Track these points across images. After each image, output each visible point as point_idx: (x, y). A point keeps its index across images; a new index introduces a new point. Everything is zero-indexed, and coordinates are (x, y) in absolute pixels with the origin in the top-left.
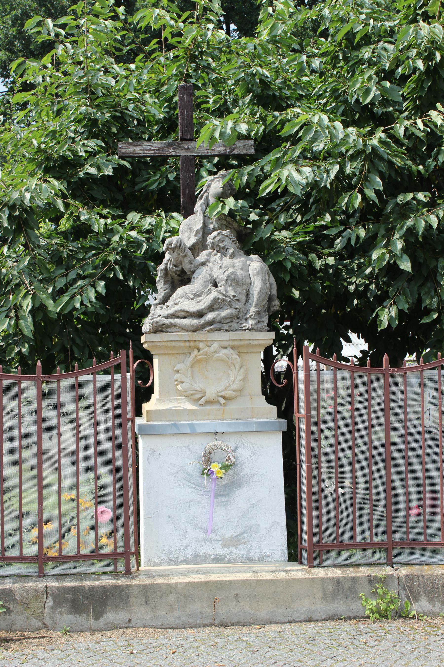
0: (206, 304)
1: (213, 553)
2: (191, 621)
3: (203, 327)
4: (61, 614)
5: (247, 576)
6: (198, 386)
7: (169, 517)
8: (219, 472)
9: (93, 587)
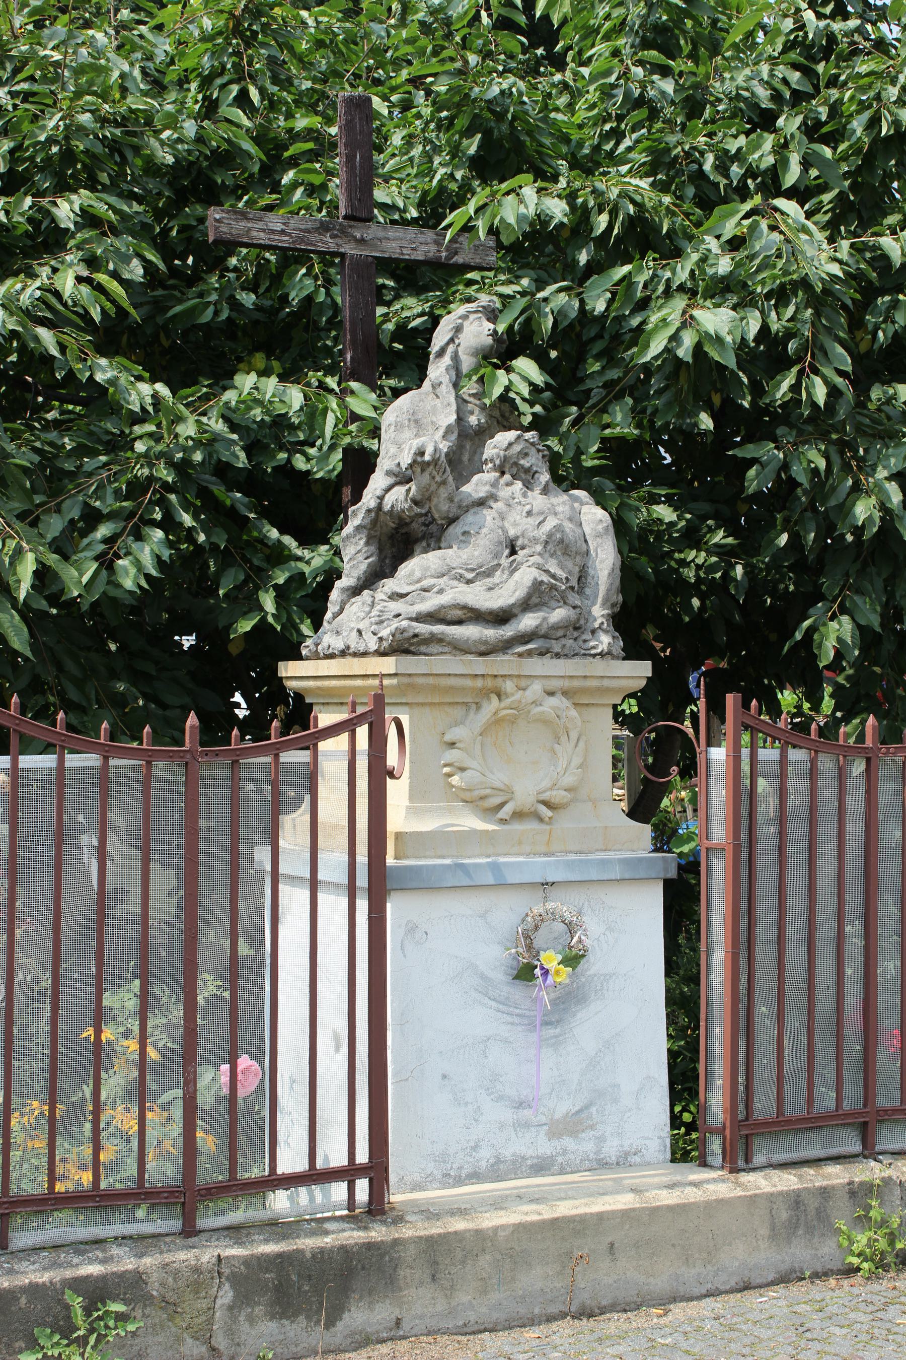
0: (517, 594)
1: (530, 1152)
2: (523, 1310)
3: (506, 646)
4: (251, 1319)
5: (624, 1201)
6: (498, 778)
7: (444, 1077)
8: (558, 973)
9: (322, 1251)
